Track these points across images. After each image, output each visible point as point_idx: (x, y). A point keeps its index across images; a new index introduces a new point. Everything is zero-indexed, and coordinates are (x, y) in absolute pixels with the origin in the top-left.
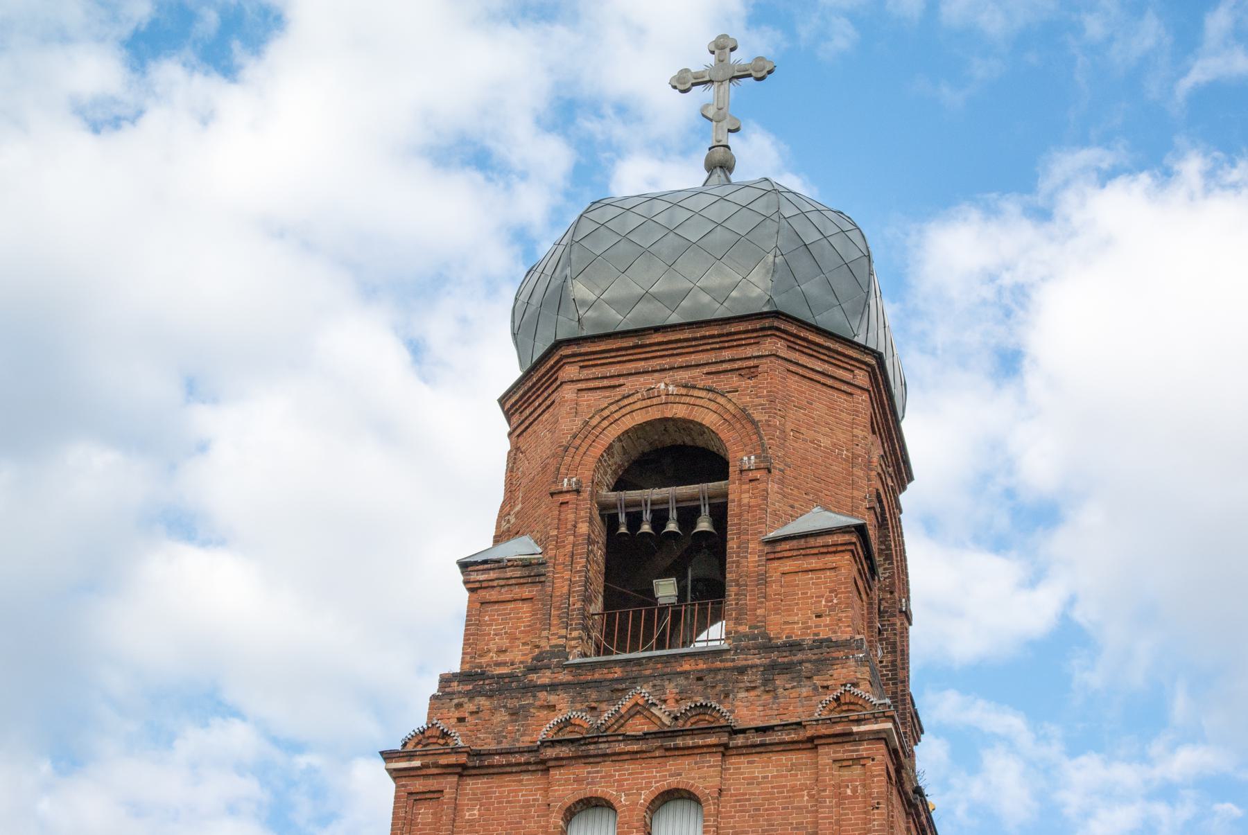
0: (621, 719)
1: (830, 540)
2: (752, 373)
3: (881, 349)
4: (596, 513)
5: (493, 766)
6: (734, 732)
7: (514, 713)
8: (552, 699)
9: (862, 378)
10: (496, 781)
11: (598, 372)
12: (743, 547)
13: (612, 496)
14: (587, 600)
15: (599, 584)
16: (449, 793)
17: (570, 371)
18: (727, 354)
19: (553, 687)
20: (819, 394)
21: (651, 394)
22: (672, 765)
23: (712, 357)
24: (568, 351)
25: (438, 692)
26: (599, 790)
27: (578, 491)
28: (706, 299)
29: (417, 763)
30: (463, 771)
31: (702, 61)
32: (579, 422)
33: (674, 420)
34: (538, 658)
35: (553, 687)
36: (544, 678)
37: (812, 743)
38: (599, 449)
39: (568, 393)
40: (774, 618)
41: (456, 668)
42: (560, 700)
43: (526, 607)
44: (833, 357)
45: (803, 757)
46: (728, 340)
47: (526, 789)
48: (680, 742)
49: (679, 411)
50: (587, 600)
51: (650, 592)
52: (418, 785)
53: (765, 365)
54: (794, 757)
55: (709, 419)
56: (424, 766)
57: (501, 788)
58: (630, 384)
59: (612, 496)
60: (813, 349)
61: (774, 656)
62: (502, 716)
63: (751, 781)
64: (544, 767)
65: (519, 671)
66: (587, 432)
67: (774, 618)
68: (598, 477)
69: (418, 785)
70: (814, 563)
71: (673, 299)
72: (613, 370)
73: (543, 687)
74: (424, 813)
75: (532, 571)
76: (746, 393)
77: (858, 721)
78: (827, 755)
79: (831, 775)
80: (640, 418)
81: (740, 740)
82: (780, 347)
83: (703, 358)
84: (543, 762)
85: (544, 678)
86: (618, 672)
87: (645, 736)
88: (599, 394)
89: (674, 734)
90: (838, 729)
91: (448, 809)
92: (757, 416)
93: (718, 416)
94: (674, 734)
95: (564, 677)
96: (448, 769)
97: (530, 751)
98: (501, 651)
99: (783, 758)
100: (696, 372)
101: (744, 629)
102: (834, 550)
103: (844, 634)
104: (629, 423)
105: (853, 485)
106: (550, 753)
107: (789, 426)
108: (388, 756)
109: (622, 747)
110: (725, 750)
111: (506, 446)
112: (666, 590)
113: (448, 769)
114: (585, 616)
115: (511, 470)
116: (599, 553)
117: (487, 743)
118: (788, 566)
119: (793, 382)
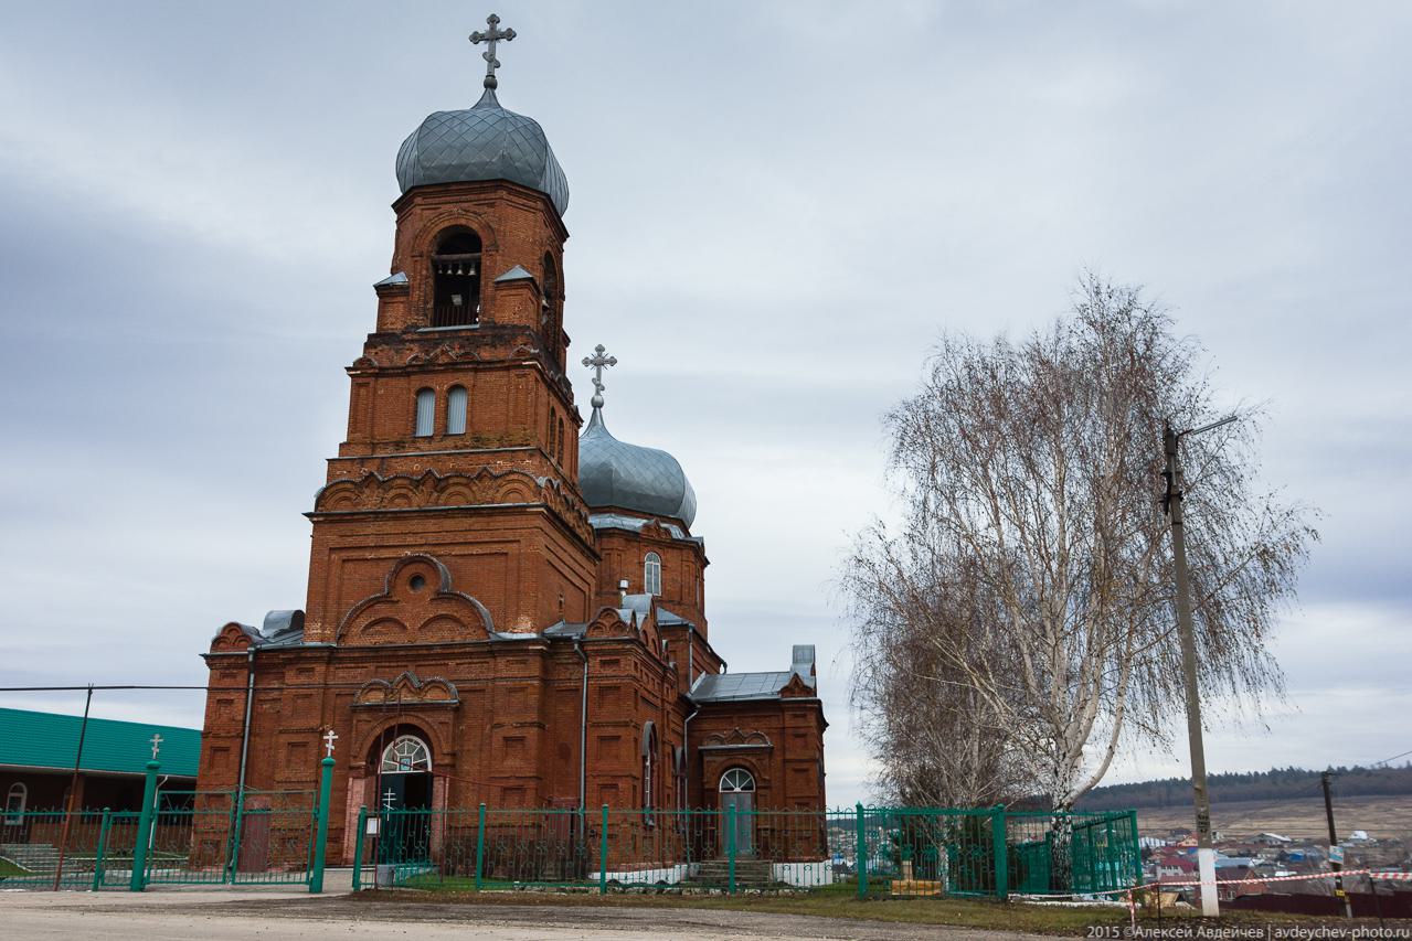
0: (437, 356)
1: (520, 283)
2: (491, 205)
3: (548, 192)
4: (430, 265)
6: (479, 363)
7: (397, 352)
8: (412, 346)
9: (540, 205)
11: (430, 201)
12: (486, 284)
13: (436, 257)
14: (426, 303)
15: (431, 294)
16: (372, 383)
17: (418, 200)
18: (483, 196)
19: (412, 341)
20: (412, 829)
21: (451, 213)
22: (457, 375)
23: (476, 197)
24: (416, 191)
25: (394, 271)
26: (429, 384)
27: (421, 256)
28: (475, 169)
30: (377, 376)
31: (484, 28)
32: (422, 225)
33: (461, 226)
34: (406, 328)
35: (412, 341)
36: (409, 337)
37: (507, 369)
38: (430, 237)
39: (418, 210)
40: (497, 315)
41: (374, 331)
42: (416, 348)
43: (402, 305)
44: (527, 197)
45: (505, 373)
46: (483, 190)
47: (402, 382)
49: (463, 222)
50: (426, 303)
51: (451, 300)
52: (360, 381)
53: (498, 202)
54: (501, 373)
55: (475, 226)
57: (394, 382)
58: (444, 208)
59: (436, 257)
60: (519, 194)
61: (497, 331)
62: (392, 352)
64: (408, 375)
65: (398, 332)
66: (425, 229)
67: (497, 315)
68: (430, 249)
69: (360, 381)
70: (513, 292)
71: (462, 167)
72: (437, 200)
73: (408, 341)
74: (363, 391)
75: (403, 290)
76: (489, 215)
77: (525, 361)
78: (513, 373)
79: (514, 380)
80: (446, 224)
81: (481, 366)
82: (504, 194)
83: (473, 197)
85: (409, 337)
86: (437, 336)
87: (445, 364)
88: (431, 212)
89: (457, 364)
90: (517, 363)
91: (371, 390)
92: (494, 226)
93: (329, 768)
95: (416, 337)
96: (372, 375)
97: (402, 368)
98: (392, 324)
99: (497, 373)
100: (469, 204)
101: (486, 319)
102: (522, 287)
103: (524, 322)
104: (442, 226)
105: (534, 254)
106: (410, 369)
107: (508, 229)
108: (348, 369)
109: (437, 368)
110: (476, 370)
111: (396, 228)
112: (457, 300)
113: (372, 375)
114: (425, 309)
115: (397, 239)
116: (431, 281)
117: (386, 364)
118: (504, 293)
119: (510, 210)
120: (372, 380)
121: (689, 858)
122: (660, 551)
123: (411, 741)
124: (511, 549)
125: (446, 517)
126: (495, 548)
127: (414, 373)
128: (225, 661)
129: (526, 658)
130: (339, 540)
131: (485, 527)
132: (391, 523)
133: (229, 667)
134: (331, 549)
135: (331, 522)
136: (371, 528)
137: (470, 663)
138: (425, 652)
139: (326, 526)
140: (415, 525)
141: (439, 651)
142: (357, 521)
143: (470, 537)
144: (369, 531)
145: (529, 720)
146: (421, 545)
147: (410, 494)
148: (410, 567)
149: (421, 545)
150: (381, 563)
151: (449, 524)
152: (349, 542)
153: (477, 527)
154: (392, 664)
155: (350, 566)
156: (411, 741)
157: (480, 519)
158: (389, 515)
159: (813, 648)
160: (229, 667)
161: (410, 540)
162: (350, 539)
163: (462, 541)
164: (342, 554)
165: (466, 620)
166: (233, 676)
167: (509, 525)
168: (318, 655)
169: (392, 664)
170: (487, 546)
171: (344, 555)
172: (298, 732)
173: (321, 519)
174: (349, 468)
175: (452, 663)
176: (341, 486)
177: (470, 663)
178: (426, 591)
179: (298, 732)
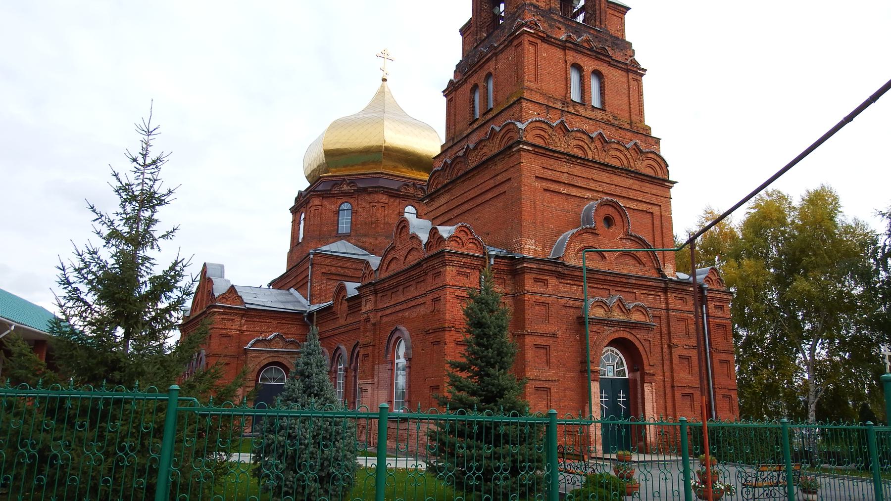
5: (551, 41)
8: (560, 26)
10: (550, 47)
29: (533, 32)
48: (600, 56)
56: (534, 33)
63: (613, 75)
84: (566, 46)
94: (599, 53)
120: (539, 41)
121: (876, 455)
122: (416, 205)
123: (612, 351)
124: (655, 209)
125: (615, 173)
126: (644, 207)
127: (570, 49)
128: (463, 260)
129: (685, 296)
130: (542, 170)
131: (639, 188)
132: (578, 167)
133: (465, 266)
134: (536, 177)
135: (536, 153)
136: (565, 168)
137: (648, 294)
138: (624, 280)
139: (532, 156)
140: (595, 174)
141: (634, 281)
142: (557, 158)
143: (631, 194)
144: (564, 169)
145: (691, 344)
146: (598, 192)
147: (586, 147)
148: (611, 209)
149: (598, 192)
150: (571, 200)
151: (617, 180)
152: (549, 174)
153: (635, 187)
154: (599, 286)
155: (548, 194)
156: (612, 351)
157: (637, 182)
158: (579, 161)
159: (222, 267)
160: (465, 266)
161: (592, 185)
162: (550, 172)
163: (625, 195)
164: (544, 184)
165: (644, 260)
166: (467, 275)
167: (654, 192)
168: (554, 269)
169: (599, 286)
170: (639, 204)
171: (545, 185)
172: (542, 335)
173: (530, 149)
174: (539, 112)
175: (638, 292)
176: (538, 124)
177: (648, 294)
178: (617, 231)
179: (542, 335)
